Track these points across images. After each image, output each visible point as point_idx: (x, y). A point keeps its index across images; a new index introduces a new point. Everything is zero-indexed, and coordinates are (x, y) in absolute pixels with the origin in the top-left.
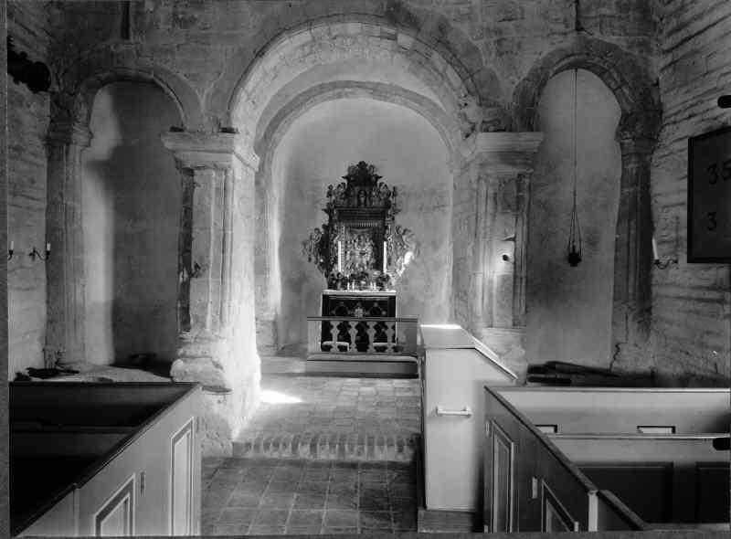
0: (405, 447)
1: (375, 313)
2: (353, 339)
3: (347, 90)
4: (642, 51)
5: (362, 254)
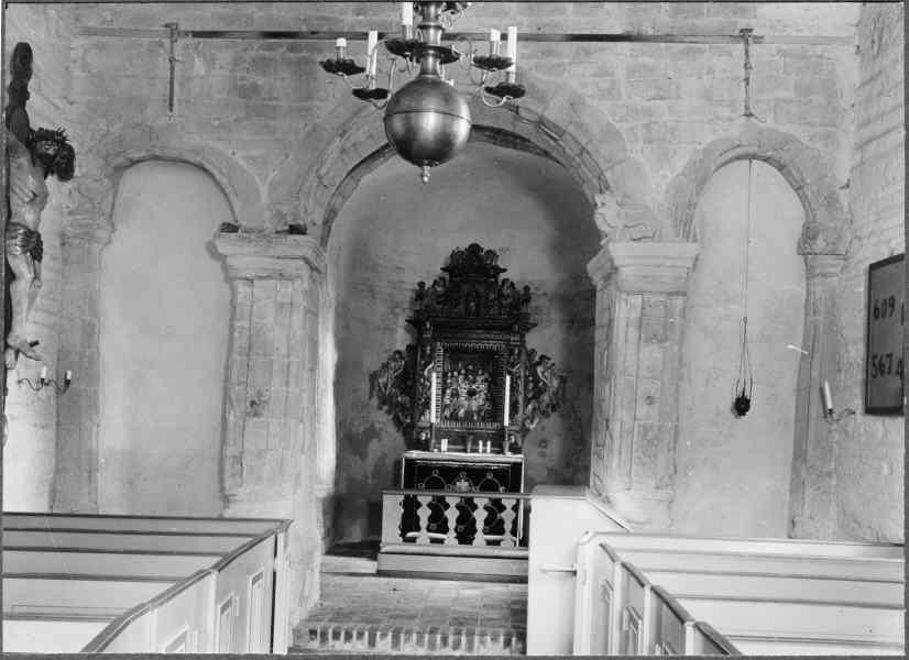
0: (514, 639)
1: (488, 487)
2: (452, 524)
4: (826, 145)
5: (472, 393)
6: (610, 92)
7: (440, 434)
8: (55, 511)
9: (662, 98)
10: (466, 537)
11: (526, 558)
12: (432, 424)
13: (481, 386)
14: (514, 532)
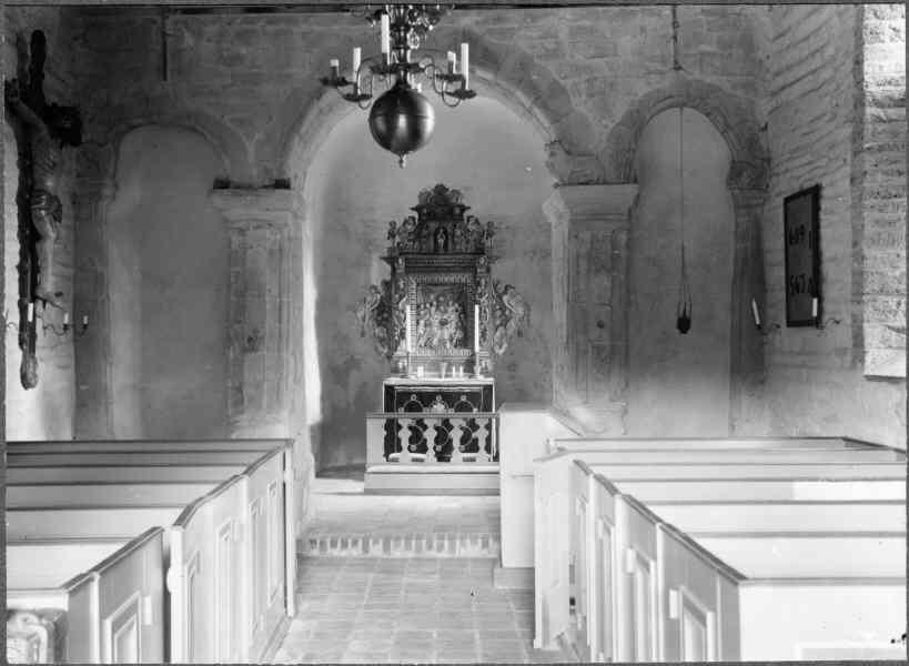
0: (491, 541)
1: (462, 408)
2: (431, 444)
5: (443, 323)
6: (554, 54)
7: (416, 361)
8: (77, 439)
10: (443, 456)
11: (498, 473)
12: (408, 353)
13: (452, 315)
14: (488, 449)
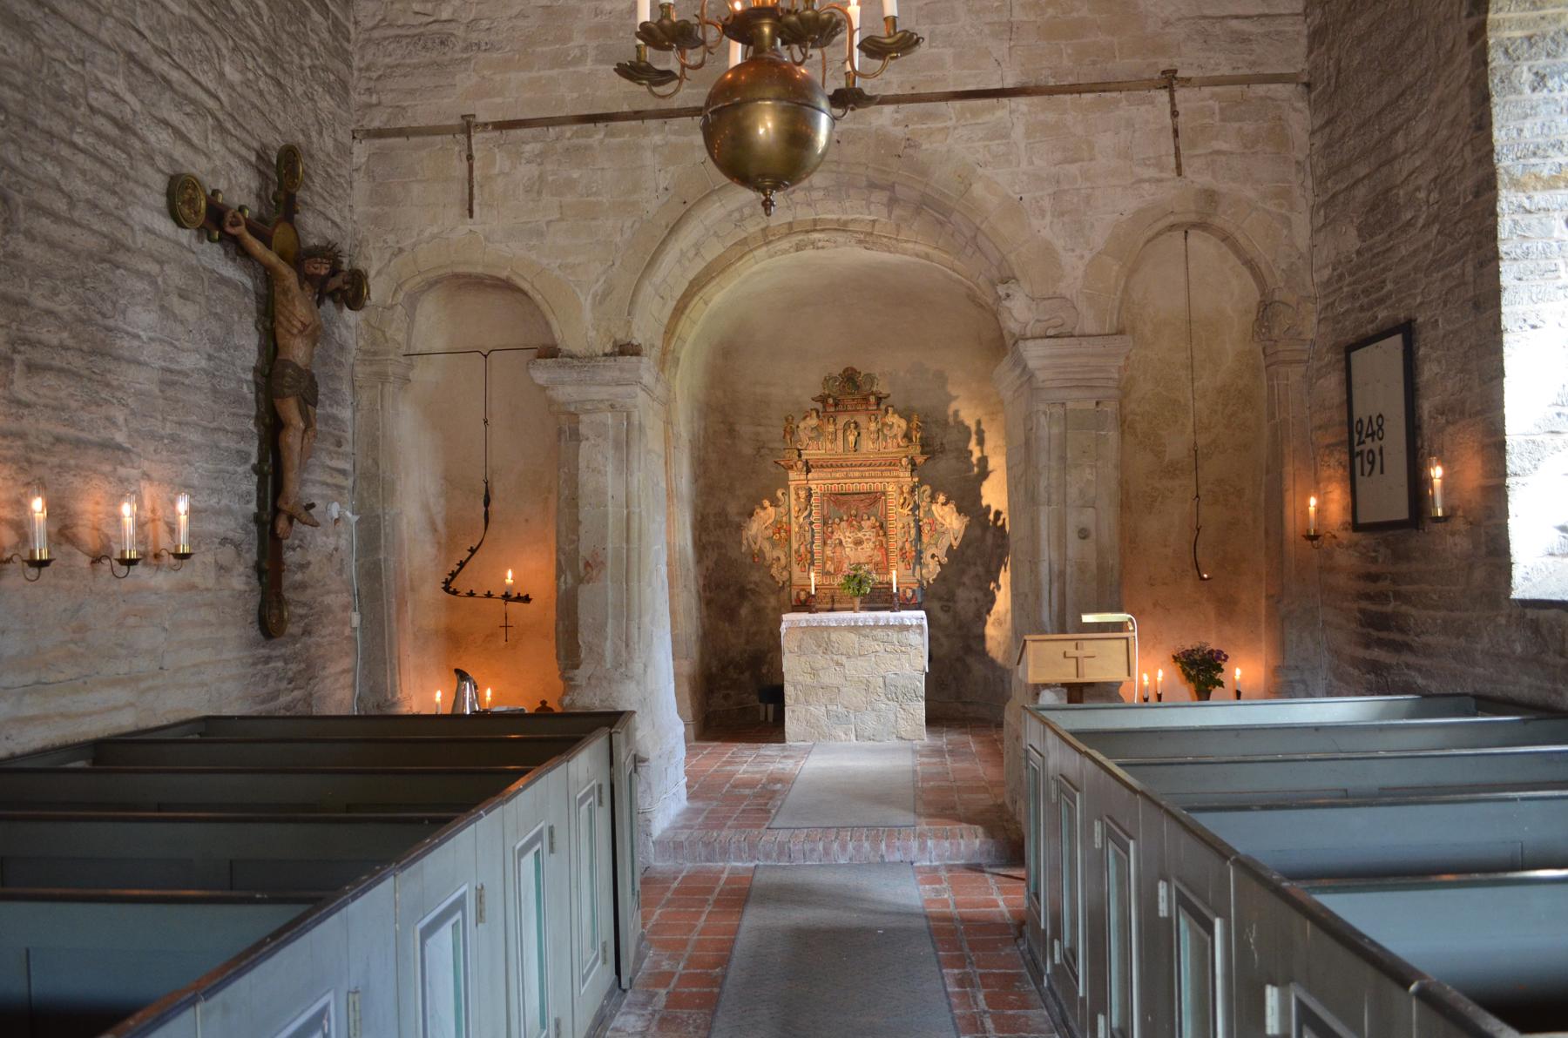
3: (816, 236)
5: (858, 543)
9: (1073, 161)
13: (868, 533)
